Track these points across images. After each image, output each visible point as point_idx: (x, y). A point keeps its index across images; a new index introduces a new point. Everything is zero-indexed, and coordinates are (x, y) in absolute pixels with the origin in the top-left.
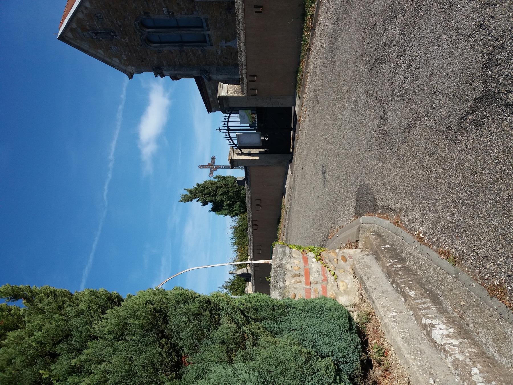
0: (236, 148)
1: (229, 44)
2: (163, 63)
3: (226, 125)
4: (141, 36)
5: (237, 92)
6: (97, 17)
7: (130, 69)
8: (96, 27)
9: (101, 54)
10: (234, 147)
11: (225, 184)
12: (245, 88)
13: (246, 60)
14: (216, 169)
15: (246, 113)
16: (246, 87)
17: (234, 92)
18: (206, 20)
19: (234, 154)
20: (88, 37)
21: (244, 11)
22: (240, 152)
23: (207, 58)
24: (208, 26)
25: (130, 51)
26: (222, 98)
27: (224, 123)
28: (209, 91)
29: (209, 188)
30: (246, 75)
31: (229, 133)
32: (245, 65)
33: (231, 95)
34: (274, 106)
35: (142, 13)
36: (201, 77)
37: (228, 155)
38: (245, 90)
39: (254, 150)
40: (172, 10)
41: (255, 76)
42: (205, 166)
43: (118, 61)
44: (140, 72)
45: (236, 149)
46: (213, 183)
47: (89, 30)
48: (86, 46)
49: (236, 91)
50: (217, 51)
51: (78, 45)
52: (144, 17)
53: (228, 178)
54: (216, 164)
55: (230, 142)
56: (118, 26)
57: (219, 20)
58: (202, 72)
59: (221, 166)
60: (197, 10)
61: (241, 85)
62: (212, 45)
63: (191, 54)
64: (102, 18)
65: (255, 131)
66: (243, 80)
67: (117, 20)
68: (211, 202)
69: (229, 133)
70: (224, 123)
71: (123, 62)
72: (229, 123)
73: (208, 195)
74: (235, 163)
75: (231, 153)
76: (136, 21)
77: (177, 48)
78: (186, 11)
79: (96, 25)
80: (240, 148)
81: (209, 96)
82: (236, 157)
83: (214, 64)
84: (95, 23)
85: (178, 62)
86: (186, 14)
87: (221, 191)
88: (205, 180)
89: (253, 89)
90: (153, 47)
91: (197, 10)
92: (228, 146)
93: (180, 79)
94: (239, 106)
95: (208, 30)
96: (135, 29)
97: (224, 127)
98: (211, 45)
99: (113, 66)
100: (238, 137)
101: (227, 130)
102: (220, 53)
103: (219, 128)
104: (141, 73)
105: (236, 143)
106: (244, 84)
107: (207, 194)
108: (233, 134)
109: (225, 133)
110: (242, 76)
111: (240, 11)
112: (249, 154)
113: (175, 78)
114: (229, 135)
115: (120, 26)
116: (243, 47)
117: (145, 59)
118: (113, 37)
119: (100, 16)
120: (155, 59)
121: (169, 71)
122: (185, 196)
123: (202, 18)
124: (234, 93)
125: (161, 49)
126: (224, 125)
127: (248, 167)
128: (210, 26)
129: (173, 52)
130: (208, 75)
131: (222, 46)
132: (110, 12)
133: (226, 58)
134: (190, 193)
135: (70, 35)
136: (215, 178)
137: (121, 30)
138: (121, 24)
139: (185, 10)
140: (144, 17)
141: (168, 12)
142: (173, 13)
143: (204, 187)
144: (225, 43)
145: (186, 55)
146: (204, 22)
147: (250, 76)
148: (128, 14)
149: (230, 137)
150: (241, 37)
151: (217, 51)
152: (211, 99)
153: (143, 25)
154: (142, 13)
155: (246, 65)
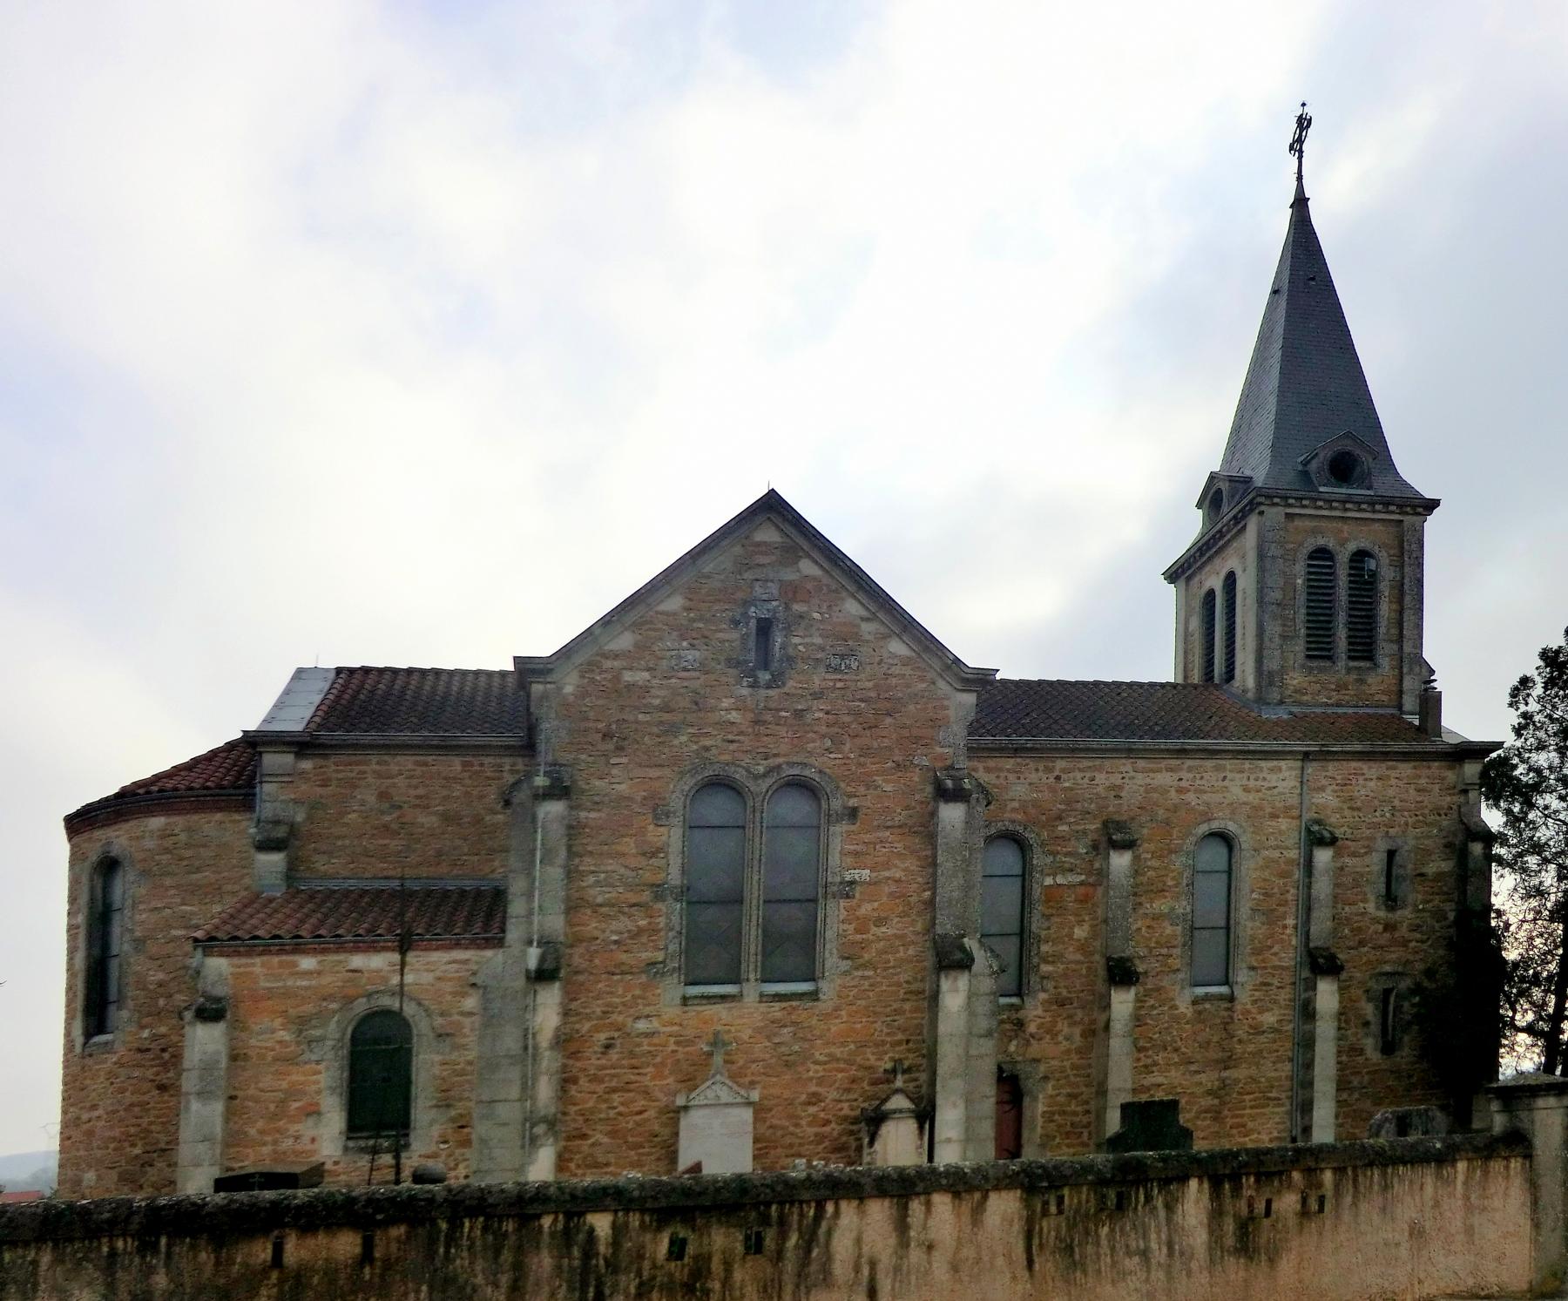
18: (814, 996)
25: (666, 708)
79: (807, 640)
84: (818, 640)
132: (863, 705)
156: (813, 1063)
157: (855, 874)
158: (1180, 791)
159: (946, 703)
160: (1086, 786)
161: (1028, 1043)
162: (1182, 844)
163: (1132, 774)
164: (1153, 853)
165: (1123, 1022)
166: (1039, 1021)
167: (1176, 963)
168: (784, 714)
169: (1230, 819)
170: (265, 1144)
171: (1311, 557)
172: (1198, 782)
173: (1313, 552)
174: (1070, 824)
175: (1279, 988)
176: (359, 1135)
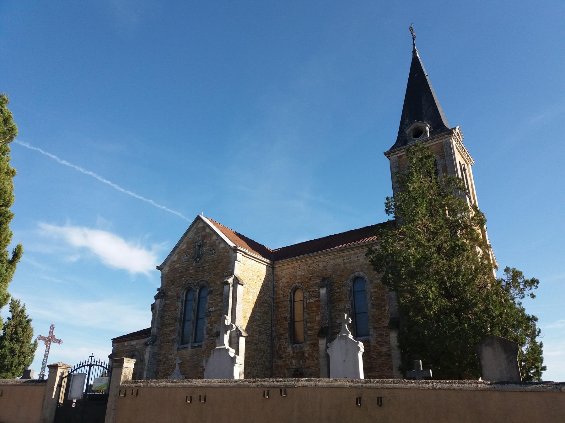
0: (70, 371)
1: (177, 367)
2: (167, 300)
3: (95, 363)
4: (193, 284)
5: (125, 377)
6: (212, 251)
7: (166, 269)
8: (205, 248)
9: (182, 247)
10: (72, 370)
11: (24, 353)
12: (127, 385)
13: (152, 387)
14: (46, 343)
15: (104, 384)
16: (129, 386)
17: (126, 374)
18: (201, 346)
19: (64, 370)
20: (198, 239)
21: (189, 387)
22: (64, 376)
23: (167, 344)
24: (195, 347)
25: (181, 272)
26: (122, 362)
27: (98, 361)
28: (135, 342)
29: (23, 334)
30: (139, 386)
31: (87, 365)
32: (147, 385)
33: (123, 371)
34: (107, 413)
35: (212, 288)
36: (150, 336)
37: (63, 363)
38: (126, 384)
39: (64, 391)
40: (211, 315)
41: (137, 394)
42: (53, 331)
43: (174, 260)
44: (162, 277)
45: (69, 372)
46: (28, 338)
47: (203, 241)
48: (190, 235)
49: (126, 375)
50: (172, 354)
51: (192, 230)
52: (209, 290)
53: (31, 357)
54: (53, 344)
55: (77, 366)
56: (204, 266)
57: (200, 359)
58: (154, 337)
59: (49, 350)
60: (210, 339)
61: (131, 381)
62: (178, 350)
63: (173, 328)
64: (211, 254)
65: (84, 391)
66: (134, 383)
67: (208, 266)
68: (3, 334)
69: (87, 365)
70: (98, 361)
71: (173, 264)
72: (97, 366)
73: (13, 331)
74: (53, 370)
75: (66, 367)
76: (206, 282)
77: (179, 316)
78: (209, 328)
79: (206, 248)
80: (69, 376)
81: (129, 342)
82: (60, 371)
83: (160, 350)
84: (208, 248)
85: (166, 315)
86: (207, 327)
87: (17, 346)
88: (34, 330)
89: (126, 392)
90: (183, 293)
91: (210, 339)
92: (73, 364)
93: (152, 312)
94: (112, 378)
95: (192, 347)
96: (199, 280)
97: (94, 362)
98: (178, 349)
99: (170, 255)
100: (81, 375)
101: (91, 363)
102: (170, 357)
103: (94, 356)
104: (161, 278)
105: (75, 372)
106: (131, 383)
107: (16, 330)
108: (85, 370)
109: (88, 362)
110: (139, 382)
111: (189, 383)
112: (60, 386)
113: (153, 307)
114: (85, 366)
115: (203, 268)
116: (161, 384)
117: (173, 284)
118: (195, 260)
119: (213, 253)
120: (172, 293)
121: (159, 305)
122: (18, 304)
123: (203, 342)
124: (125, 374)
125: (180, 300)
126: (96, 361)
127: (46, 384)
128: (195, 349)
129: (177, 312)
130: (150, 344)
131: (176, 359)
132: (215, 262)
133: (164, 363)
134: (21, 310)
135: (201, 225)
136: (36, 341)
137: (200, 267)
138: (205, 269)
139: (211, 327)
140: (209, 290)
141: (211, 311)
142: (209, 316)
143: (26, 328)
144: (179, 364)
145: (172, 324)
146: (199, 344)
147: (138, 390)
148: (212, 276)
149: (83, 366)
150: (170, 383)
151: (172, 355)
152: (126, 344)
153: (202, 288)
154: (212, 289)
155: (147, 387)
156: (200, 367)
158: (345, 264)
159: (231, 257)
160: (317, 267)
161: (305, 361)
162: (346, 283)
163: (330, 261)
164: (337, 287)
165: (323, 352)
166: (308, 352)
168: (201, 268)
169: (361, 271)
170: (298, 283)
172: (349, 260)
175: (386, 336)
176: (72, 379)
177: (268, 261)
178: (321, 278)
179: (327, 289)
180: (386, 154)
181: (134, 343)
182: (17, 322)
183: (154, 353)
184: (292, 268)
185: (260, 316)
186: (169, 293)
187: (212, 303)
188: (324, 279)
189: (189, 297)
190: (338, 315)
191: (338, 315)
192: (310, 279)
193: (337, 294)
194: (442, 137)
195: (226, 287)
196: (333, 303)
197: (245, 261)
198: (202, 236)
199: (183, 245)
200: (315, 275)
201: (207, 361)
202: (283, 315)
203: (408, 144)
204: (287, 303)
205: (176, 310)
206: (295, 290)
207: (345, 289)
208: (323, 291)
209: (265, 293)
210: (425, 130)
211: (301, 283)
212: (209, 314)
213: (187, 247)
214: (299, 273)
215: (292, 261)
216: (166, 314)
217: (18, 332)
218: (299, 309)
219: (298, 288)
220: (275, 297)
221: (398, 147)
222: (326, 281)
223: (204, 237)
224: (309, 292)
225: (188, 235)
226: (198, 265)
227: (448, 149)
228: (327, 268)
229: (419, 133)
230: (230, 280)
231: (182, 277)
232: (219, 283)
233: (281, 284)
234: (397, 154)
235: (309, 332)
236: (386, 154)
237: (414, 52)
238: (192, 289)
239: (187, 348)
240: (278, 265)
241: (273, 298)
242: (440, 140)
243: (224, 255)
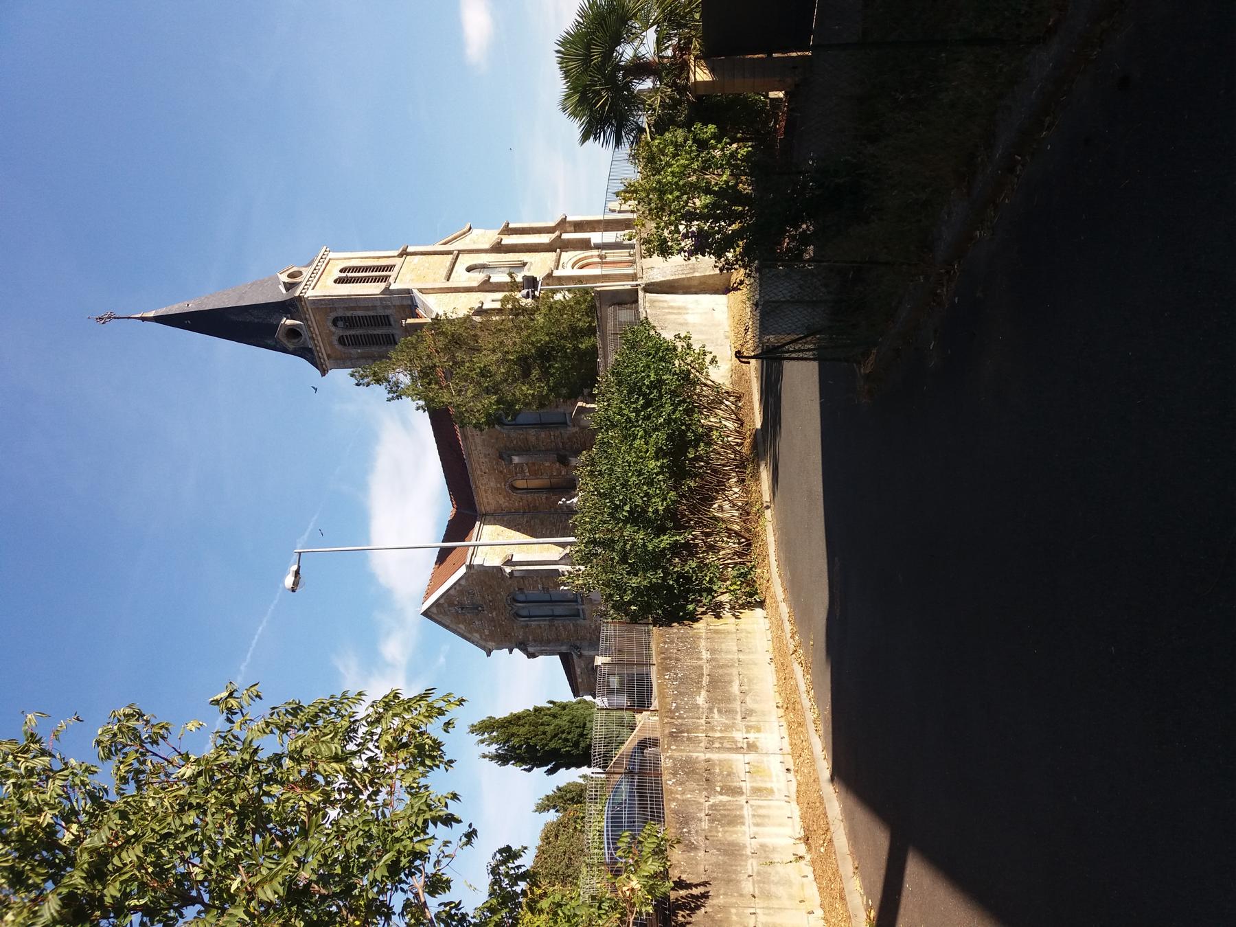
7: (490, 644)
24: (582, 601)
25: (495, 626)
47: (456, 605)
48: (447, 621)
71: (484, 637)
76: (508, 596)
77: (547, 623)
98: (585, 619)
99: (473, 642)
115: (490, 601)
125: (529, 623)
135: (434, 610)
145: (556, 629)
152: (580, 680)
154: (517, 589)
157: (568, 581)
167: (557, 433)
170: (505, 485)
171: (345, 345)
173: (341, 344)
174: (504, 469)
177: (478, 524)
178: (500, 460)
179: (513, 455)
180: (323, 374)
181: (578, 671)
182: (561, 800)
183: (589, 645)
184: (486, 492)
185: (547, 529)
186: (520, 637)
187: (533, 588)
188: (501, 457)
189: (524, 613)
190: (543, 443)
191: (543, 443)
192: (501, 472)
193: (520, 443)
194: (305, 309)
195: (516, 574)
196: (529, 448)
197: (482, 553)
198: (449, 606)
199: (460, 628)
200: (495, 467)
201: (595, 601)
202: (544, 501)
203: (310, 347)
204: (530, 497)
205: (540, 627)
206: (514, 488)
207: (513, 434)
208: (516, 459)
209: (518, 524)
210: (444, 597)
211: (506, 482)
212: (545, 589)
213: (463, 624)
214: (492, 484)
215: (478, 492)
216: (545, 638)
217: (571, 797)
218: (535, 483)
219: (512, 486)
220: (522, 511)
221: (313, 358)
222: (503, 455)
223: (451, 604)
224: (516, 473)
225: (447, 624)
226: (487, 607)
227: (323, 302)
228: (487, 453)
229: (293, 332)
230: (508, 570)
231: (501, 625)
232: (510, 582)
233: (507, 504)
234: (324, 360)
235: (563, 473)
236: (323, 374)
237: (144, 319)
238: (515, 613)
239: (583, 610)
240: (482, 509)
241: (524, 513)
242: (308, 311)
243: (475, 579)
